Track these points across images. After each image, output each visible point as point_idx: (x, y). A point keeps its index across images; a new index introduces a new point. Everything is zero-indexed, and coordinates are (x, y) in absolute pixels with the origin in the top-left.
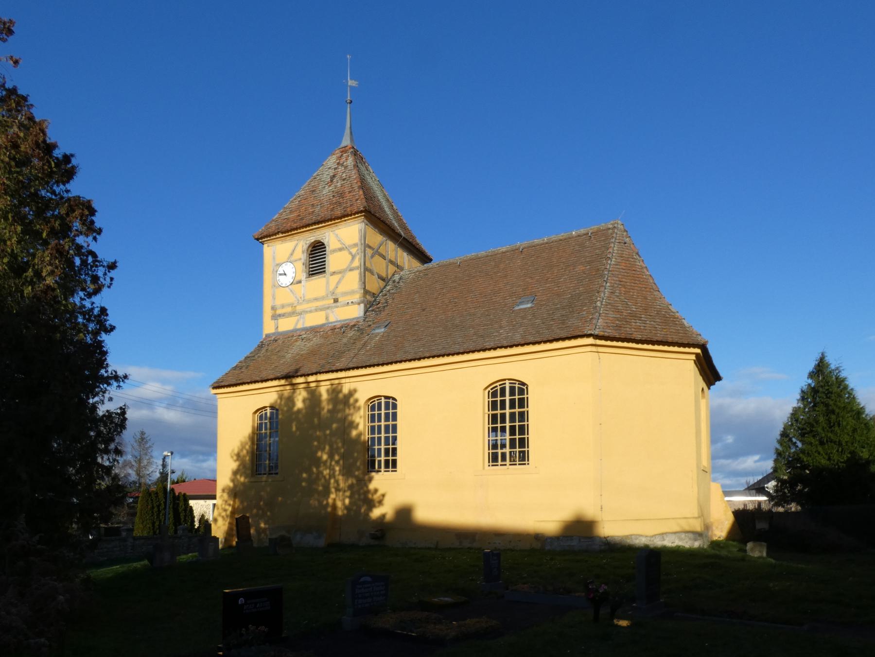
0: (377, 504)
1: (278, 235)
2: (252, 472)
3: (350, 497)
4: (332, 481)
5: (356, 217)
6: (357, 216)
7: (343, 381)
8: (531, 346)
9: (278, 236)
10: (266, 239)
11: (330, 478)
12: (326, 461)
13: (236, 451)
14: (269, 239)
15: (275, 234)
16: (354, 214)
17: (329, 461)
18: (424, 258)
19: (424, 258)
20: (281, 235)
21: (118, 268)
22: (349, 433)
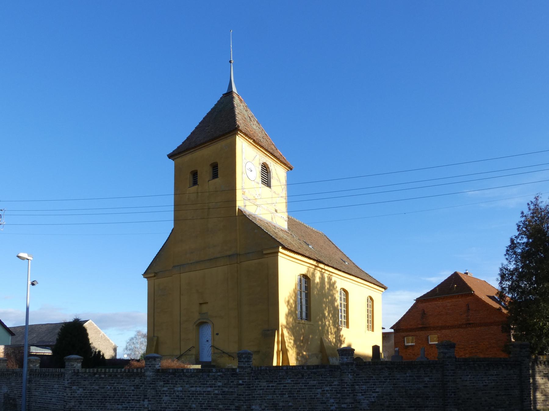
0: (343, 343)
1: (251, 140)
2: (295, 319)
3: (335, 338)
4: (329, 328)
5: (284, 167)
6: (287, 168)
7: (333, 275)
8: (372, 284)
9: (249, 140)
10: (242, 135)
11: (329, 327)
12: (327, 317)
13: (287, 299)
14: (244, 136)
15: (250, 138)
16: (287, 166)
17: (328, 317)
18: (18, 257)
19: (18, 257)
20: (251, 141)
21: (461, 272)
22: (334, 304)
